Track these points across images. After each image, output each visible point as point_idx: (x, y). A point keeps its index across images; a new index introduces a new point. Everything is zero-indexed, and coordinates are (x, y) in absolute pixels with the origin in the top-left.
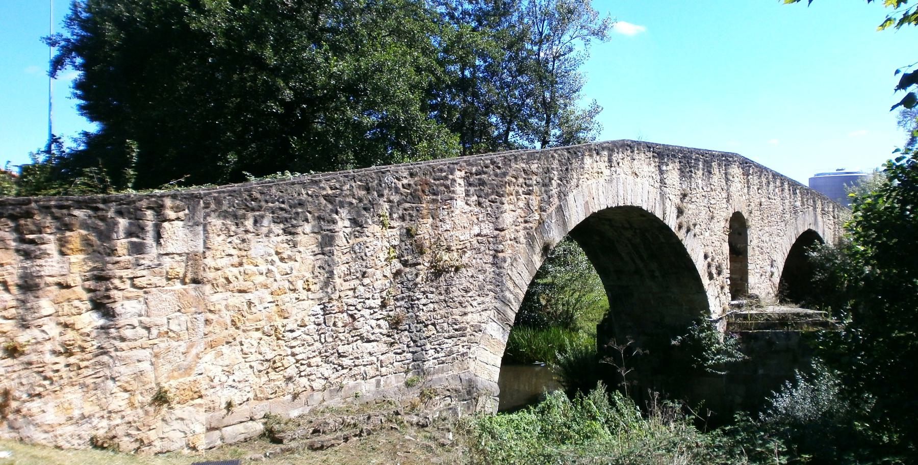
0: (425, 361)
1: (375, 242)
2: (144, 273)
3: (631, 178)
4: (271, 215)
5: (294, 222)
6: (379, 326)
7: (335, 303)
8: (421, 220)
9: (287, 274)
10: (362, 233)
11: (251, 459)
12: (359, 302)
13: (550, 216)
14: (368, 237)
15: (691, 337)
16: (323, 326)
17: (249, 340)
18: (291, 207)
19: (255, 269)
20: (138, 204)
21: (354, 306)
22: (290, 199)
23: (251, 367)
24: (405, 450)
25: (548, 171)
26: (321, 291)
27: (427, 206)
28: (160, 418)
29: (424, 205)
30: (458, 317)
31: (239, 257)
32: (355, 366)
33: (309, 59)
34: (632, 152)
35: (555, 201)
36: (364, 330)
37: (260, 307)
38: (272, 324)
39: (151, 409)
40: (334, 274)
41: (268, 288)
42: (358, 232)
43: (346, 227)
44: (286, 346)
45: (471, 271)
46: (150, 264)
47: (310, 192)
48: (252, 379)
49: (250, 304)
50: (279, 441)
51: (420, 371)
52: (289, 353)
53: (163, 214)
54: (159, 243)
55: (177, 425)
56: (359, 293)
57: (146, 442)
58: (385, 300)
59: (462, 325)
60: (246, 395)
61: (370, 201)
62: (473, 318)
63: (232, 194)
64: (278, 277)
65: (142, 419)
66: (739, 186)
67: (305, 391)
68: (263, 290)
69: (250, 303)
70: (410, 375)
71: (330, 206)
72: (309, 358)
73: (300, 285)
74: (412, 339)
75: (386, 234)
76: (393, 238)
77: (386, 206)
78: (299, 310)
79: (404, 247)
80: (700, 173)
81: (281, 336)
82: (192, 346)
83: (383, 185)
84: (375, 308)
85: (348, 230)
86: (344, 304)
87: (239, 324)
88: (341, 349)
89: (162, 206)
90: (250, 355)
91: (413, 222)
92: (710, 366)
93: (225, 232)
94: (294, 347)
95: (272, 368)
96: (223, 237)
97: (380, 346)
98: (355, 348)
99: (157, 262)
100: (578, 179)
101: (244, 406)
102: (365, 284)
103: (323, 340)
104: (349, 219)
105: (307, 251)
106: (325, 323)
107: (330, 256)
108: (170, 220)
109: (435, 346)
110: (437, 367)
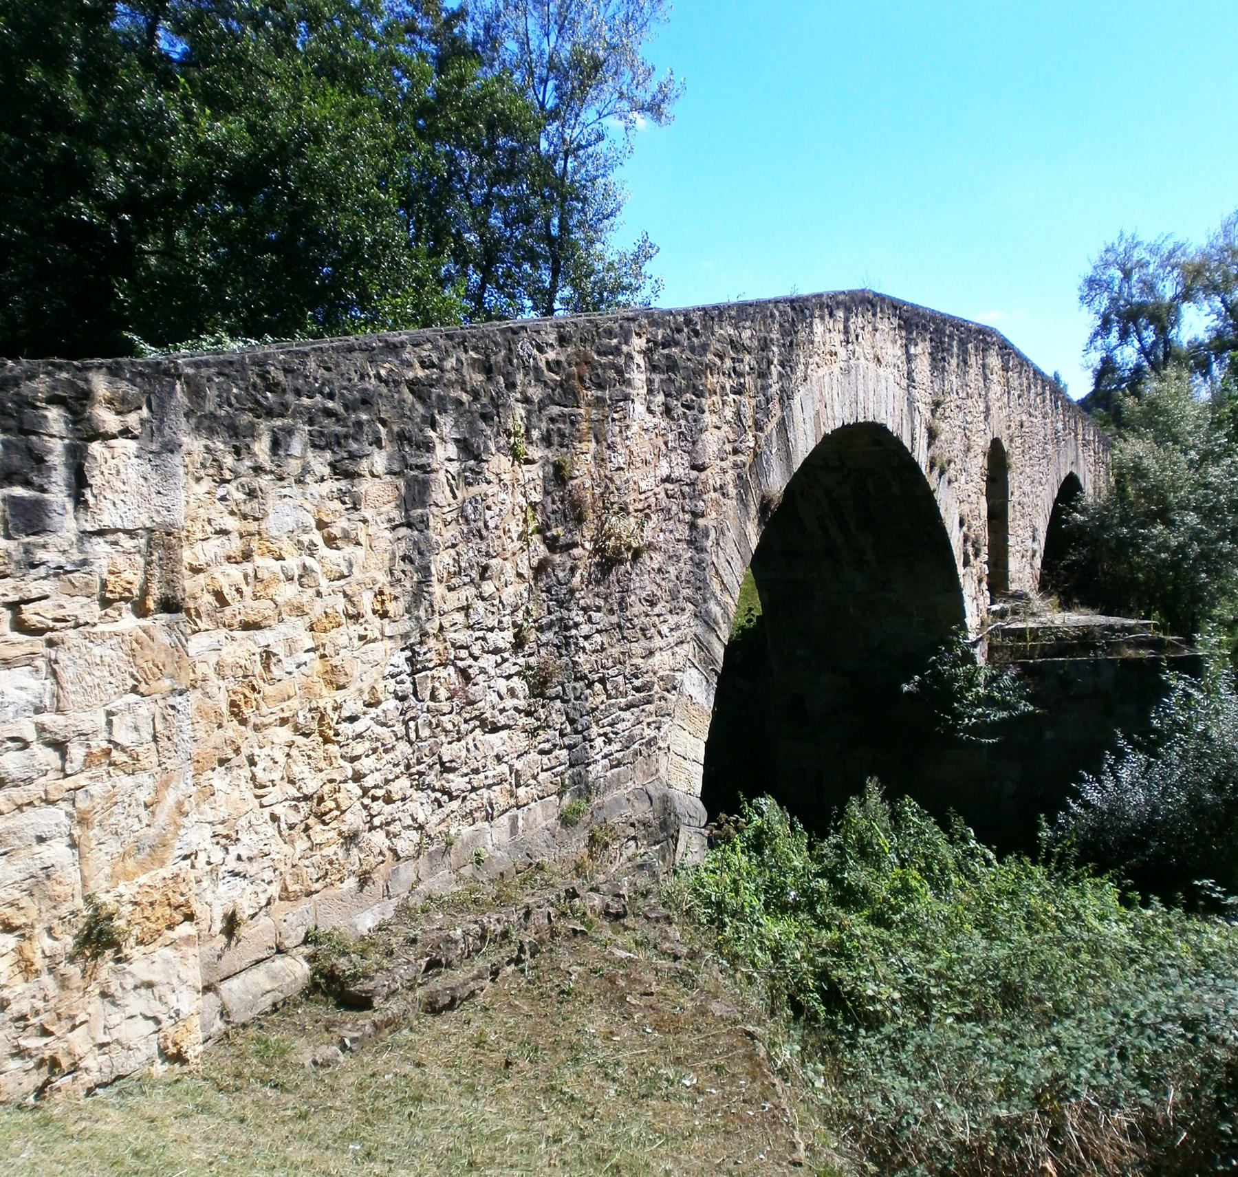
0: (588, 765)
1: (502, 496)
2: (47, 586)
3: (872, 365)
4: (307, 428)
5: (354, 446)
6: (512, 693)
7: (432, 642)
8: (578, 446)
9: (342, 577)
10: (479, 473)
11: (315, 1063)
12: (477, 639)
13: (769, 438)
14: (489, 483)
15: (937, 676)
16: (412, 700)
17: (266, 750)
18: (346, 407)
19: (276, 566)
20: (26, 388)
21: (467, 648)
22: (345, 388)
23: (274, 818)
24: (640, 989)
25: (765, 345)
26: (407, 616)
27: (587, 412)
28: (97, 991)
29: (582, 411)
30: (639, 661)
31: (241, 537)
32: (474, 789)
33: (148, 113)
34: (874, 315)
35: (775, 408)
36: (487, 704)
37: (288, 664)
38: (314, 705)
39: (74, 971)
40: (431, 575)
41: (304, 614)
42: (472, 471)
43: (450, 460)
44: (342, 757)
45: (657, 559)
46: (62, 560)
47: (383, 372)
48: (278, 848)
49: (268, 657)
50: (362, 1003)
51: (584, 789)
52: (350, 773)
53: (89, 419)
54: (80, 502)
55: (137, 1003)
56: (476, 617)
57: (65, 1062)
58: (520, 631)
59: (647, 678)
60: (265, 891)
61: (492, 398)
62: (663, 662)
63: (227, 371)
64: (324, 585)
65: (52, 1003)
66: (998, 388)
67: (383, 862)
68: (294, 619)
69: (268, 656)
70: (567, 799)
71: (420, 409)
72: (387, 782)
73: (367, 602)
74: (568, 718)
75: (520, 476)
76: (532, 485)
77: (520, 410)
78: (367, 667)
79: (550, 507)
80: (954, 361)
81: (331, 733)
82: (166, 784)
83: (515, 361)
84: (505, 650)
85: (454, 467)
86: (448, 645)
87: (247, 712)
88: (447, 753)
89: (86, 396)
90: (271, 789)
91: (565, 450)
92: (967, 729)
93: (211, 471)
94: (358, 758)
95: (316, 816)
96: (207, 484)
97: (515, 738)
98: (471, 746)
99: (77, 556)
100: (806, 365)
101: (263, 921)
102: (486, 595)
103: (413, 736)
104: (456, 441)
105: (378, 519)
106: (415, 693)
107: (421, 531)
108: (106, 437)
109: (605, 730)
110: (608, 774)
